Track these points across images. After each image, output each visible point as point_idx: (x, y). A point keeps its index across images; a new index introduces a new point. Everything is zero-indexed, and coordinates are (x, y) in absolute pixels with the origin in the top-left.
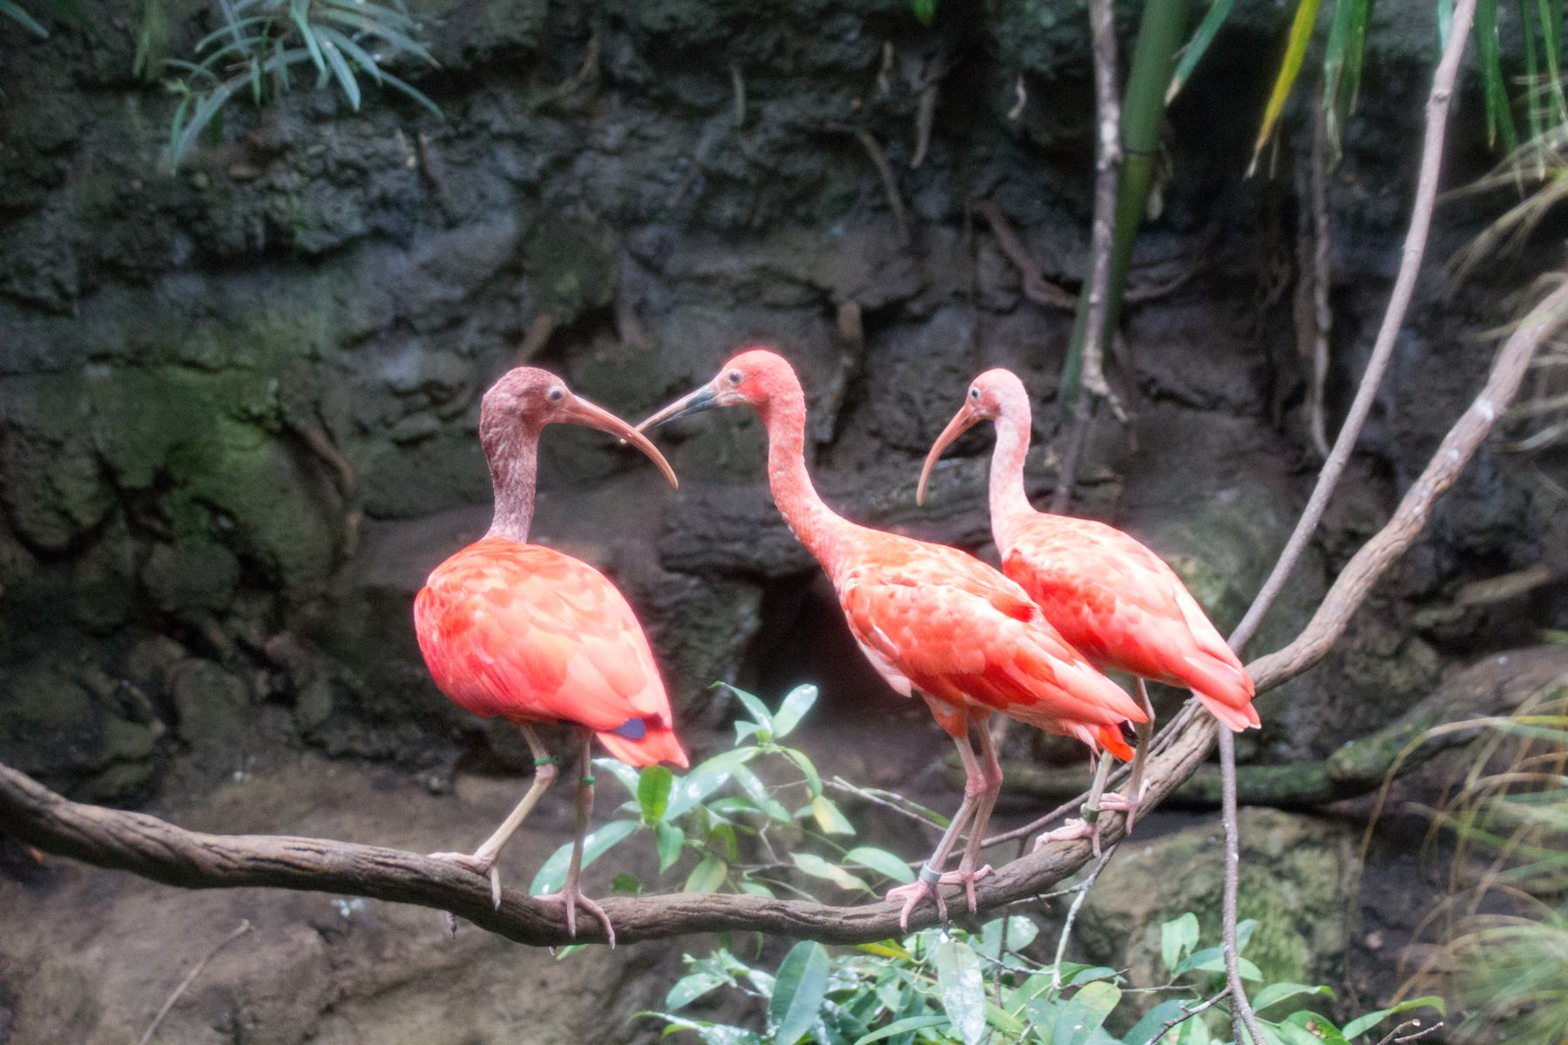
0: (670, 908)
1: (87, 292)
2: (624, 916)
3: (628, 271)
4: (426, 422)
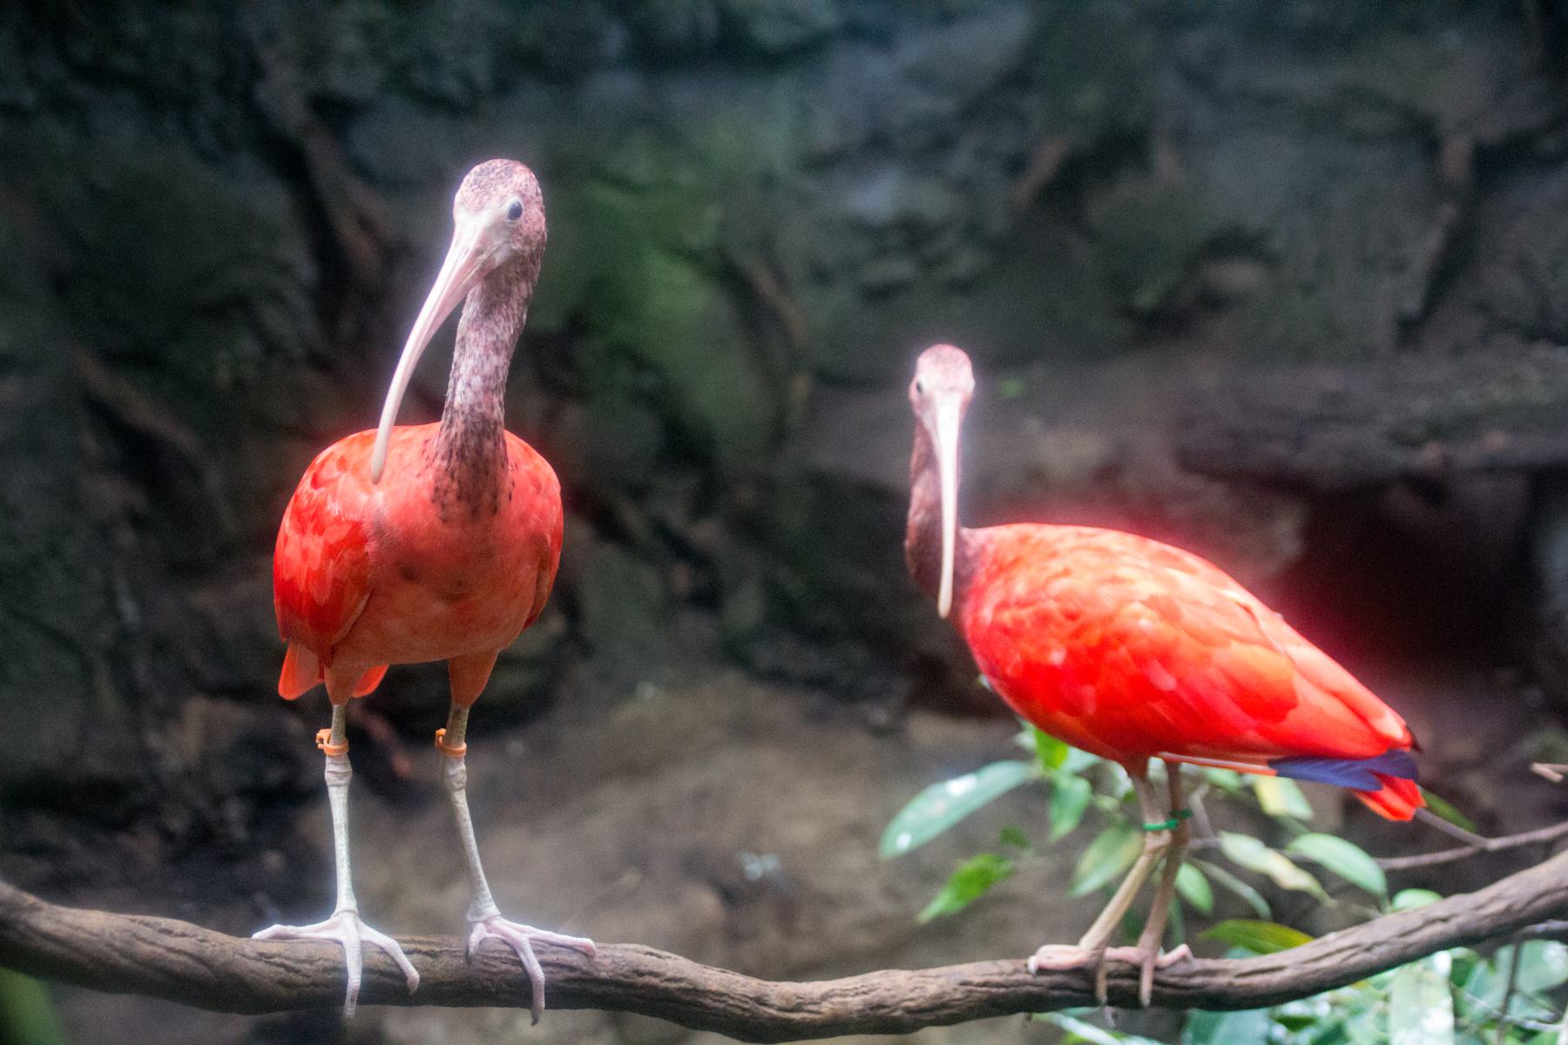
0: (964, 984)
1: (502, 87)
2: (893, 997)
3: (1168, 88)
4: (899, 268)
